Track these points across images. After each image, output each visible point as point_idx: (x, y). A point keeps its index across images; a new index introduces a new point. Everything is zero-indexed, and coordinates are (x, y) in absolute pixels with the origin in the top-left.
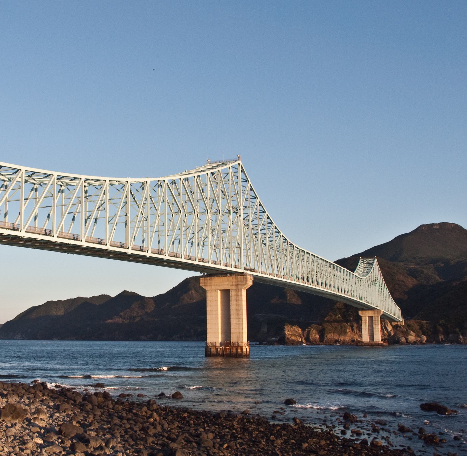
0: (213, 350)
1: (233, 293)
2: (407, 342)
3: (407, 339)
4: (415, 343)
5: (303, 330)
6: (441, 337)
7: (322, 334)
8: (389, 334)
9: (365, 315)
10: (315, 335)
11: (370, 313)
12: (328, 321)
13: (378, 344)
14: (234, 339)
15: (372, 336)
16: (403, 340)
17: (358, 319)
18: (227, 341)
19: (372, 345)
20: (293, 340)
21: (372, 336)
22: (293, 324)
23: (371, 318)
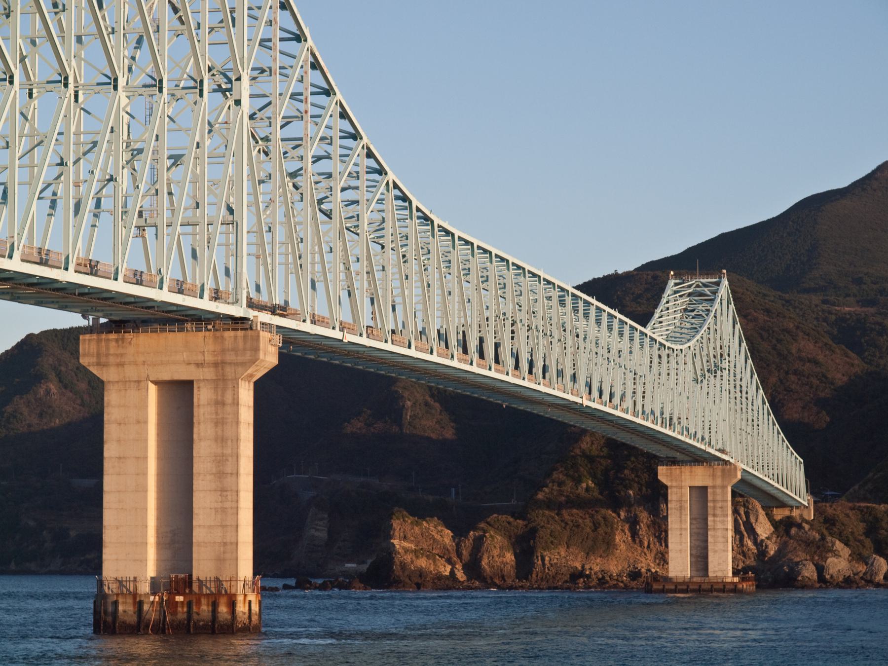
0: (126, 608)
1: (203, 396)
2: (823, 581)
3: (820, 570)
4: (848, 582)
5: (459, 533)
6: (13, 566)
7: (525, 548)
8: (762, 552)
9: (679, 482)
10: (499, 555)
11: (698, 476)
12: (549, 504)
13: (723, 588)
14: (203, 568)
15: (701, 558)
16: (809, 572)
17: (658, 494)
18: (178, 579)
19: (702, 590)
20: (421, 573)
21: (701, 558)
22: (420, 512)
23: (701, 493)
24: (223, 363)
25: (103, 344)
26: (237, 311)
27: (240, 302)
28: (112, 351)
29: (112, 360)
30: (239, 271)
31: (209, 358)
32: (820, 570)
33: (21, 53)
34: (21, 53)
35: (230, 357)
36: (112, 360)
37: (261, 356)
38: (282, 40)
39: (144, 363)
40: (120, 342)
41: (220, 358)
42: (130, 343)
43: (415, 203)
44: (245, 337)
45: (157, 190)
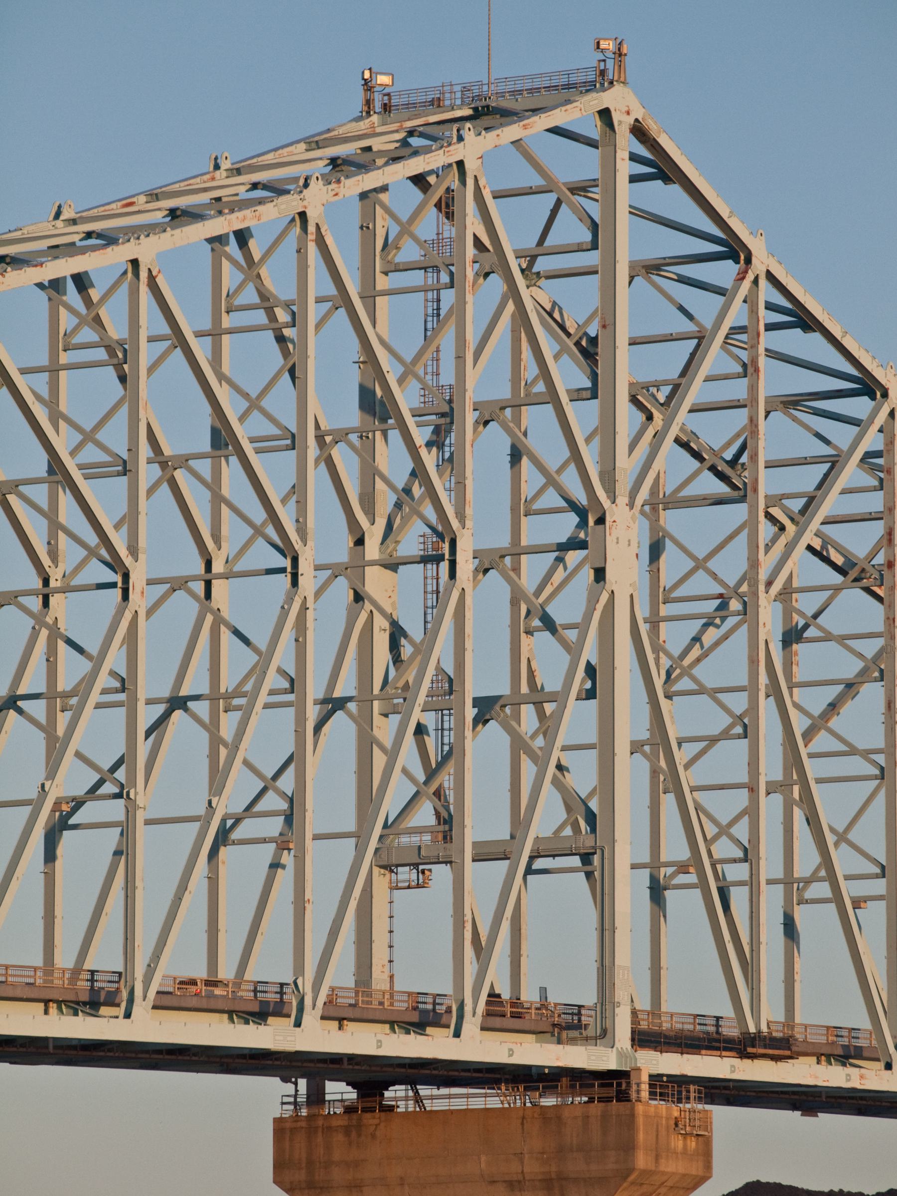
6: (665, 1079)
24: (562, 1178)
25: (320, 1139)
26: (603, 1059)
27: (609, 1035)
28: (337, 1156)
29: (338, 1175)
30: (607, 962)
31: (532, 1168)
32: (316, 1097)
33: (317, 426)
34: (317, 426)
35: (575, 1166)
36: (338, 1175)
37: (642, 1161)
38: (770, 327)
39: (402, 1182)
40: (354, 1134)
41: (554, 1169)
42: (373, 1136)
43: (762, 261)
44: (605, 1117)
45: (882, 671)
